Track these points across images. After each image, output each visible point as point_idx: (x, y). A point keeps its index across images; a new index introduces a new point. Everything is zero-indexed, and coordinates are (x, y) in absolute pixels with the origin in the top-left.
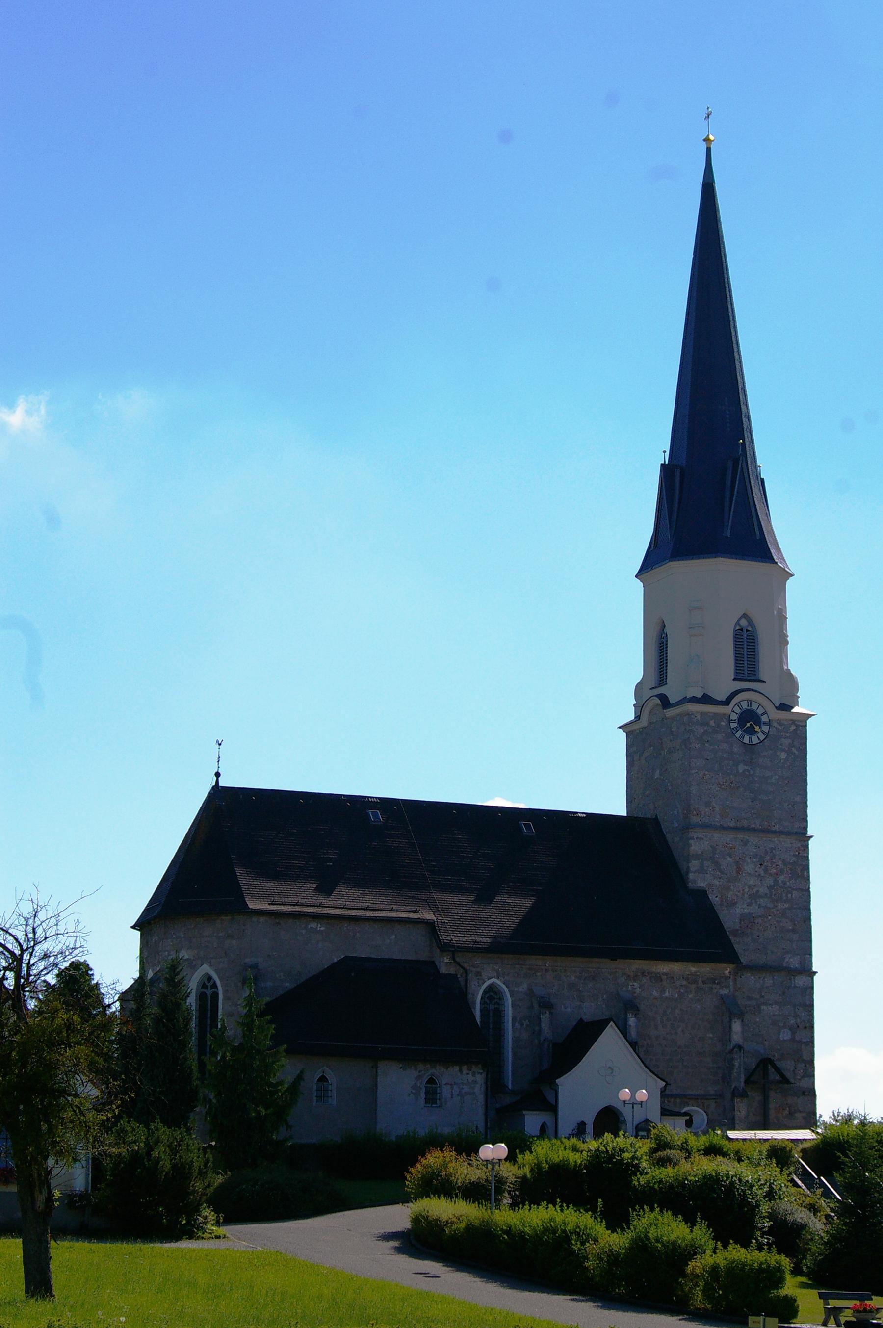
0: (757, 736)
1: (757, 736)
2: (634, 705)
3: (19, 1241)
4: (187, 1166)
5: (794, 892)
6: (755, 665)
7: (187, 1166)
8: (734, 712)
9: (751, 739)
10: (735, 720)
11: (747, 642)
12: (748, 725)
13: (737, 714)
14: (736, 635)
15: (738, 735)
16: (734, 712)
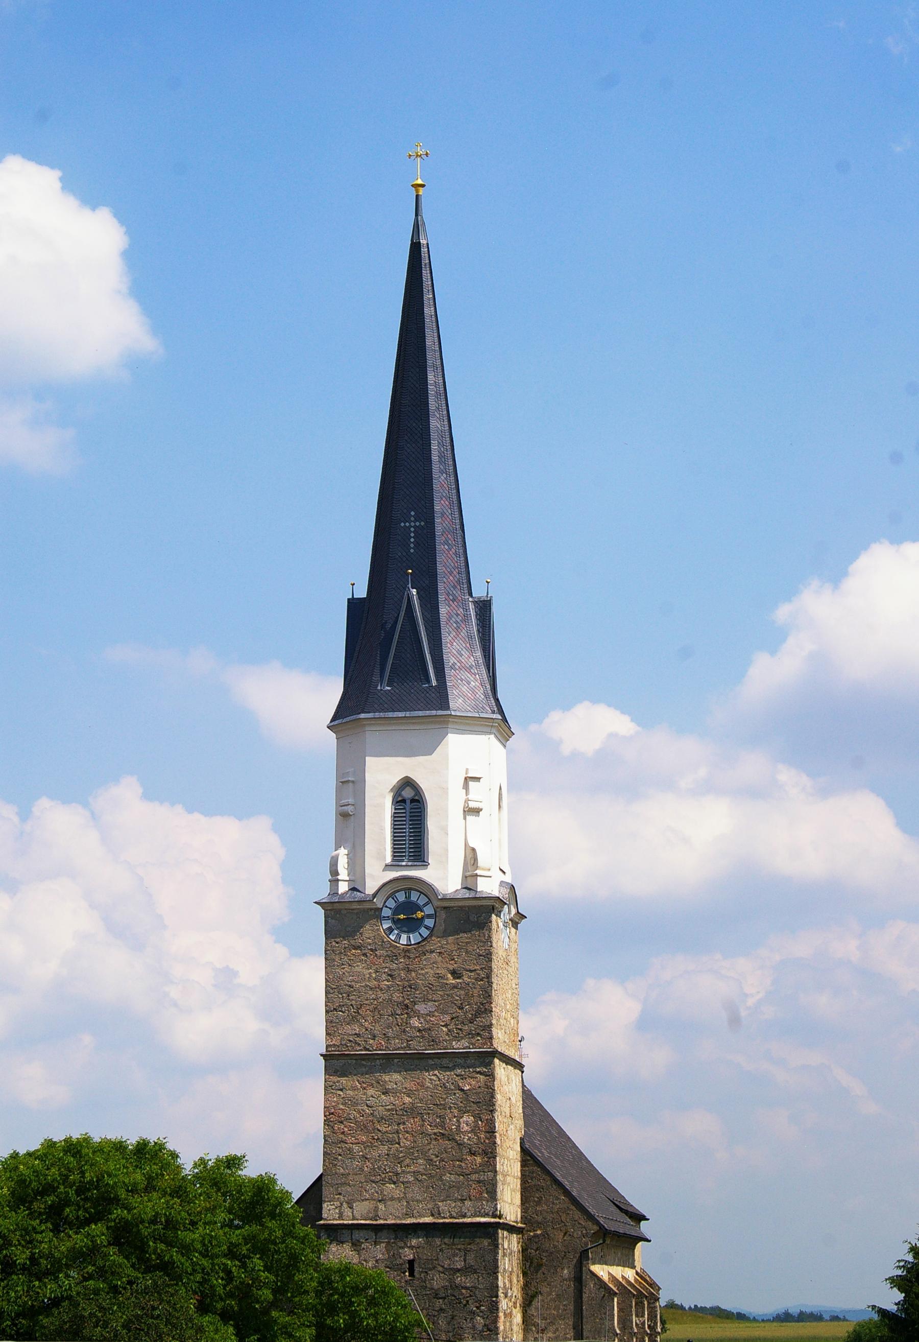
3: (365, 596)
8: (386, 907)
10: (388, 917)
13: (390, 908)
16: (386, 907)
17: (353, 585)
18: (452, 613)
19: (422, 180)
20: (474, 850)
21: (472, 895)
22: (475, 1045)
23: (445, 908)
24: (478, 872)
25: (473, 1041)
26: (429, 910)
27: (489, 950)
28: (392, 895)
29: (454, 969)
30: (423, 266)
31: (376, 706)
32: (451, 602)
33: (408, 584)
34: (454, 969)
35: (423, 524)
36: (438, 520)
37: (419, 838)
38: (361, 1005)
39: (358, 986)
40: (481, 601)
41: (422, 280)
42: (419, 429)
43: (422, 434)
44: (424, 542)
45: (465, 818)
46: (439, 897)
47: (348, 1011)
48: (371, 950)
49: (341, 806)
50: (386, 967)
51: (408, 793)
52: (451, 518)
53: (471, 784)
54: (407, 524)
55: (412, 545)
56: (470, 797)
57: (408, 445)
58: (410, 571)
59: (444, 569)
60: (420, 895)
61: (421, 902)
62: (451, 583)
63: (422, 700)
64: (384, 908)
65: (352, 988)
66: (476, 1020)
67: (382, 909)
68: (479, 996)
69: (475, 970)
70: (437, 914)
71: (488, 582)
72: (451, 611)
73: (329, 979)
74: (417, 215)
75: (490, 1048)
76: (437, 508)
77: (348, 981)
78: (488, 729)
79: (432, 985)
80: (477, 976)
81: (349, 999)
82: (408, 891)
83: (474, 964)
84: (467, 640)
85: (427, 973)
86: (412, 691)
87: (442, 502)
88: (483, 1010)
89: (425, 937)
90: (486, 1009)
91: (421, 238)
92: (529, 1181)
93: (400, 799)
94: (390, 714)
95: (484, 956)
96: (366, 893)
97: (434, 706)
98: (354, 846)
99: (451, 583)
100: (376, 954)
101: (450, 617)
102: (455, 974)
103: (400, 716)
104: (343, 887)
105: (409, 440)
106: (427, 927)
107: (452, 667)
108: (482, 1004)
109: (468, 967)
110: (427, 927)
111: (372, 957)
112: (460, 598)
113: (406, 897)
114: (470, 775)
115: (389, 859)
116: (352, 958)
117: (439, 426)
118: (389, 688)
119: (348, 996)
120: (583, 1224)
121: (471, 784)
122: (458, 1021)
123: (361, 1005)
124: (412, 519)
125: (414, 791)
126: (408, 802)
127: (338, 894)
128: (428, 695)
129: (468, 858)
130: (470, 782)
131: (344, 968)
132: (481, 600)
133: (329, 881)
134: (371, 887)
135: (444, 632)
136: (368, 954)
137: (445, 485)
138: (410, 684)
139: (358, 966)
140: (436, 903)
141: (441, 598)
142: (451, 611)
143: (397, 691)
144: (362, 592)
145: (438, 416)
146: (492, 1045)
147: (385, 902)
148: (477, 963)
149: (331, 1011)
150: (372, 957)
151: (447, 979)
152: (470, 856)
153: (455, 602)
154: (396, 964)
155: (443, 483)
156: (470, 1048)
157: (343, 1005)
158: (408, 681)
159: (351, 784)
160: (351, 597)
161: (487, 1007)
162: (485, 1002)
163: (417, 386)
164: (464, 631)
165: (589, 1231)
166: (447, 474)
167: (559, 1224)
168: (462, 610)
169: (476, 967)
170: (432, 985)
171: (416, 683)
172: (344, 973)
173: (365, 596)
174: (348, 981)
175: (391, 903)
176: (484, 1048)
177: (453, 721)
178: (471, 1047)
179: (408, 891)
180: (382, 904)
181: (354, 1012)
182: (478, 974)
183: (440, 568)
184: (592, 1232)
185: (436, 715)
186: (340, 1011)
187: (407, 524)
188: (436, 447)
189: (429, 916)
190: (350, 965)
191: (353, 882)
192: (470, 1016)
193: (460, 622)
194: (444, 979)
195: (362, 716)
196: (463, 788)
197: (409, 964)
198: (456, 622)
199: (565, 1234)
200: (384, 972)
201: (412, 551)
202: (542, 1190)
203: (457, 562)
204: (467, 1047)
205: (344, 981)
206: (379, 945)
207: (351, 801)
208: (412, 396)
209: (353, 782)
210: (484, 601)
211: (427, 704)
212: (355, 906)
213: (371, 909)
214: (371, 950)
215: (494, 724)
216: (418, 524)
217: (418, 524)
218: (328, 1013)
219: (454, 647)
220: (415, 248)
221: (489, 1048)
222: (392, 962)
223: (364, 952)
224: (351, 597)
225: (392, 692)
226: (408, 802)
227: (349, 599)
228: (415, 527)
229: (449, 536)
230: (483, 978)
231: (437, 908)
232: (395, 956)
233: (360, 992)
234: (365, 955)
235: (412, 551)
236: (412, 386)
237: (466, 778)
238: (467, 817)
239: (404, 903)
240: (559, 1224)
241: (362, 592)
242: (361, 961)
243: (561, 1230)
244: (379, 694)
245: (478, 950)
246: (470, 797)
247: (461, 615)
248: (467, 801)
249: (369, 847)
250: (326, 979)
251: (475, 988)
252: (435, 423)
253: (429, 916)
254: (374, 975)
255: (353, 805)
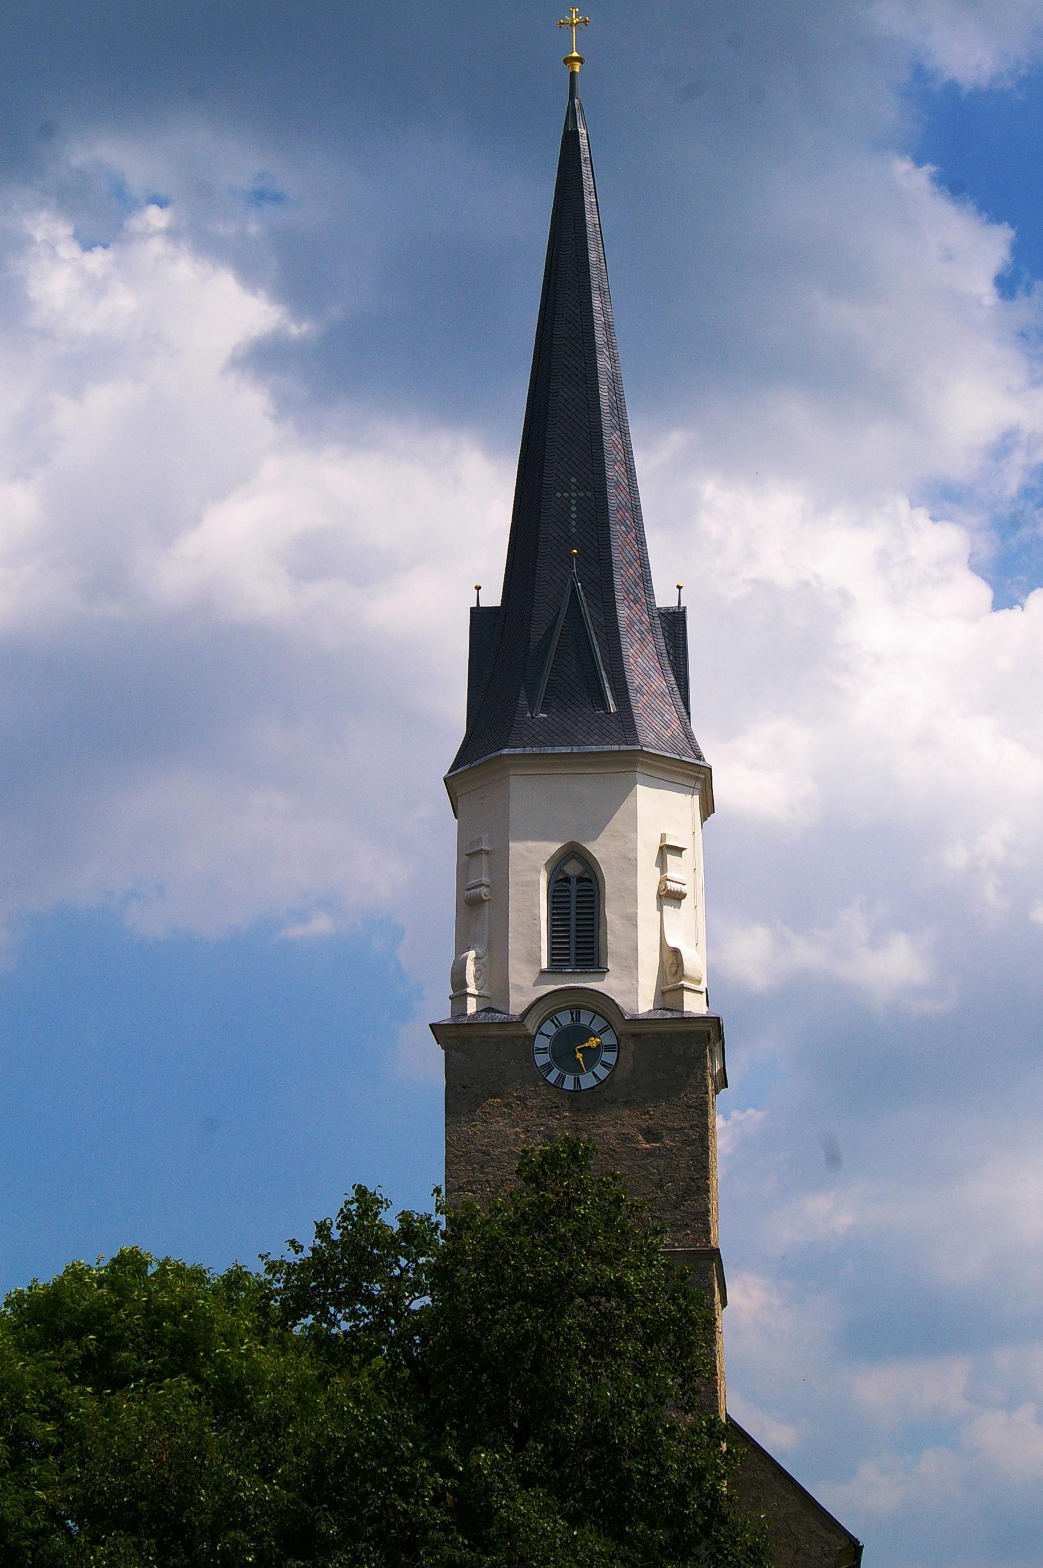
0: (593, 1073)
1: (593, 1073)
2: (478, 615)
3: (499, 605)
4: (78, 1470)
5: (403, 1265)
6: (592, 908)
7: (78, 1470)
8: (542, 1034)
9: (577, 1081)
10: (544, 1049)
11: (568, 891)
12: (579, 1056)
13: (548, 1036)
14: (555, 891)
15: (552, 1078)
16: (542, 1034)
17: (478, 588)
18: (634, 619)
19: (578, 54)
20: (676, 952)
21: (676, 1015)
22: (682, 1242)
23: (634, 1035)
24: (684, 983)
25: (679, 1235)
26: (609, 1039)
27: (703, 1098)
28: (551, 1016)
29: (648, 1127)
30: (582, 161)
31: (525, 739)
32: (631, 603)
33: (573, 569)
34: (648, 1127)
35: (589, 494)
36: (611, 491)
37: (592, 928)
38: (502, 1182)
39: (497, 1153)
40: (670, 613)
41: (582, 178)
42: (581, 369)
43: (585, 376)
44: (592, 519)
45: (660, 909)
46: (626, 1018)
47: (482, 1190)
48: (519, 1098)
49: (468, 890)
50: (542, 1124)
51: (573, 869)
52: (628, 490)
53: (671, 859)
54: (566, 495)
55: (574, 523)
56: (669, 874)
57: (566, 390)
58: (575, 551)
59: (622, 558)
60: (595, 1016)
61: (596, 1027)
62: (631, 578)
63: (596, 731)
64: (538, 1035)
65: (489, 1155)
66: (683, 1205)
67: (535, 1036)
68: (688, 1167)
69: (682, 1128)
70: (622, 1045)
71: (679, 587)
72: (632, 616)
73: (451, 1142)
74: (572, 97)
75: (707, 1246)
76: (609, 473)
77: (482, 1145)
78: (692, 783)
79: (614, 1151)
80: (685, 1138)
81: (483, 1173)
82: (576, 1010)
83: (679, 1119)
84: (656, 658)
85: (606, 1133)
86: (580, 719)
87: (616, 467)
88: (694, 1189)
89: (602, 1079)
90: (698, 1187)
91: (578, 126)
92: (740, 1472)
93: (561, 877)
94: (549, 750)
95: (695, 1108)
96: (511, 1013)
97: (616, 739)
98: (489, 947)
99: (631, 578)
100: (526, 1105)
101: (631, 624)
102: (651, 1135)
103: (564, 751)
104: (472, 1006)
105: (566, 383)
106: (605, 1065)
107: (638, 691)
108: (693, 1180)
109: (669, 1124)
110: (605, 1065)
111: (520, 1108)
112: (644, 601)
113: (572, 1019)
114: (668, 843)
115: (544, 965)
116: (488, 1110)
117: (609, 367)
118: (545, 716)
119: (482, 1167)
120: (825, 1536)
121: (671, 859)
122: (655, 1205)
123: (502, 1182)
124: (573, 487)
125: (582, 864)
126: (574, 881)
127: (467, 1014)
128: (604, 725)
129: (667, 965)
130: (668, 856)
131: (476, 1125)
132: (671, 611)
133: (450, 998)
134: (518, 1003)
135: (625, 640)
136: (513, 1105)
137: (619, 446)
138: (577, 710)
139: (497, 1122)
140: (620, 1027)
141: (619, 595)
142: (632, 616)
143: (557, 719)
144: (493, 597)
145: (607, 353)
146: (710, 1243)
147: (540, 1027)
148: (685, 1117)
149: (455, 1191)
150: (520, 1108)
151: (638, 1142)
152: (669, 959)
153: (637, 605)
154: (556, 1119)
155: (617, 443)
156: (674, 1247)
157: (474, 1182)
158: (573, 707)
159: (484, 857)
160: (475, 605)
161: (700, 1185)
162: (698, 1176)
163: (577, 312)
164: (650, 645)
165: (833, 1548)
166: (621, 432)
167: (787, 1537)
168: (647, 616)
169: (683, 1125)
170: (614, 1151)
171: (584, 709)
172: (475, 1133)
173: (499, 605)
174: (482, 1145)
175: (550, 1029)
176: (696, 1247)
177: (644, 762)
178: (676, 1245)
179: (576, 1010)
180: (535, 1030)
181: (490, 1191)
182: (688, 1135)
183: (616, 555)
184: (839, 1547)
185: (619, 751)
186: (469, 1191)
187: (566, 495)
188: (607, 394)
189: (609, 1048)
190: (485, 1122)
191: (488, 1001)
192: (674, 1197)
193: (645, 633)
194: (633, 1143)
195: (505, 751)
196: (656, 866)
197: (577, 1120)
198: (641, 632)
199: (798, 1551)
200: (539, 1132)
201: (574, 530)
202: (760, 1486)
203: (638, 551)
204: (670, 1244)
205: (474, 1145)
206: (530, 1091)
207: (485, 880)
208: (570, 325)
209: (487, 853)
210: (674, 613)
211: (603, 737)
212: (494, 1032)
213: (518, 1037)
214: (519, 1098)
215: (700, 776)
216: (581, 494)
217: (581, 494)
218: (450, 1193)
219: (638, 664)
220: (571, 139)
221: (704, 1247)
222: (551, 1116)
223: (507, 1101)
224: (475, 605)
225: (549, 720)
226: (574, 881)
227: (472, 609)
228: (578, 498)
229: (626, 514)
230: (694, 1140)
231: (622, 1035)
232: (555, 1107)
233: (500, 1162)
234: (508, 1105)
235: (574, 530)
236: (570, 312)
237: (661, 848)
238: (665, 907)
239: (568, 1029)
240: (787, 1537)
241: (493, 597)
242: (502, 1115)
243: (790, 1546)
244: (530, 723)
245: (685, 1099)
246: (669, 874)
247: (646, 623)
248: (664, 880)
249: (515, 945)
250: (446, 1141)
251: (681, 1156)
252: (603, 363)
253: (609, 1048)
254: (522, 1136)
255: (488, 886)
